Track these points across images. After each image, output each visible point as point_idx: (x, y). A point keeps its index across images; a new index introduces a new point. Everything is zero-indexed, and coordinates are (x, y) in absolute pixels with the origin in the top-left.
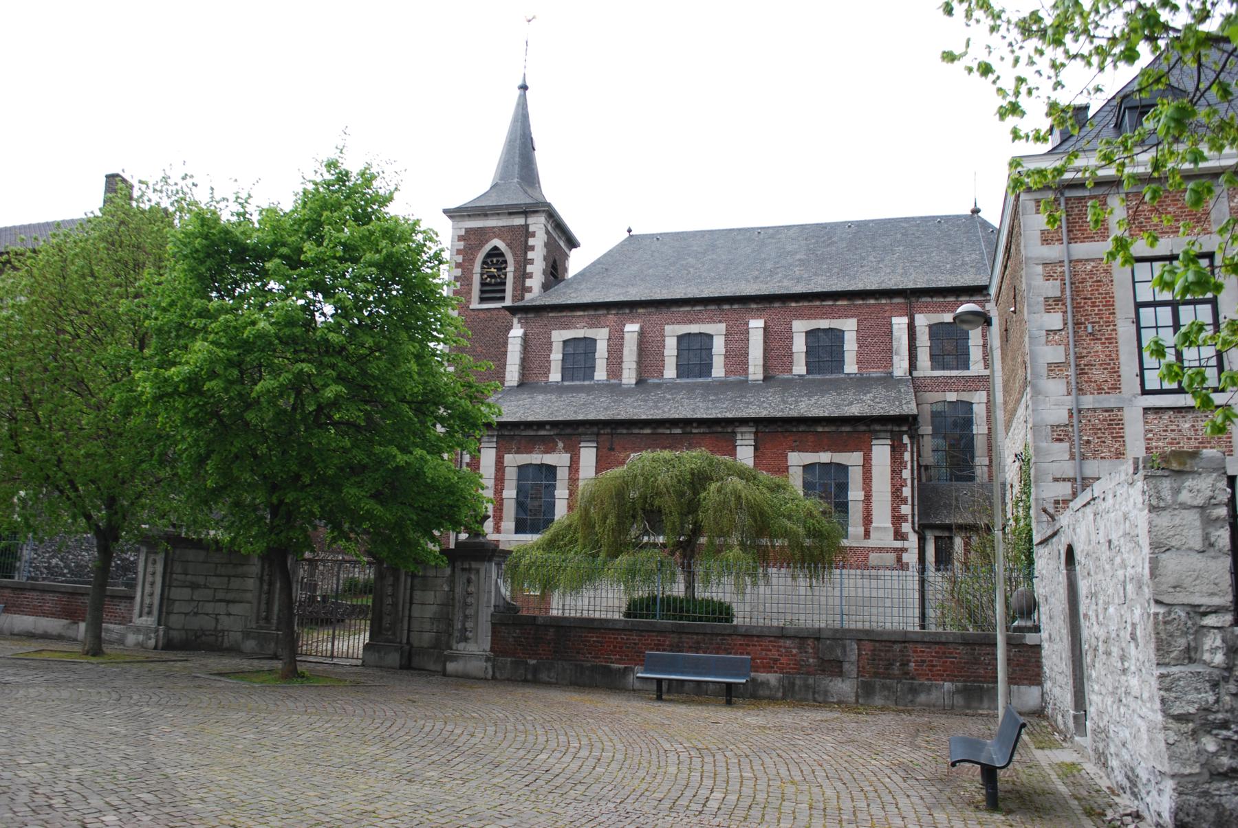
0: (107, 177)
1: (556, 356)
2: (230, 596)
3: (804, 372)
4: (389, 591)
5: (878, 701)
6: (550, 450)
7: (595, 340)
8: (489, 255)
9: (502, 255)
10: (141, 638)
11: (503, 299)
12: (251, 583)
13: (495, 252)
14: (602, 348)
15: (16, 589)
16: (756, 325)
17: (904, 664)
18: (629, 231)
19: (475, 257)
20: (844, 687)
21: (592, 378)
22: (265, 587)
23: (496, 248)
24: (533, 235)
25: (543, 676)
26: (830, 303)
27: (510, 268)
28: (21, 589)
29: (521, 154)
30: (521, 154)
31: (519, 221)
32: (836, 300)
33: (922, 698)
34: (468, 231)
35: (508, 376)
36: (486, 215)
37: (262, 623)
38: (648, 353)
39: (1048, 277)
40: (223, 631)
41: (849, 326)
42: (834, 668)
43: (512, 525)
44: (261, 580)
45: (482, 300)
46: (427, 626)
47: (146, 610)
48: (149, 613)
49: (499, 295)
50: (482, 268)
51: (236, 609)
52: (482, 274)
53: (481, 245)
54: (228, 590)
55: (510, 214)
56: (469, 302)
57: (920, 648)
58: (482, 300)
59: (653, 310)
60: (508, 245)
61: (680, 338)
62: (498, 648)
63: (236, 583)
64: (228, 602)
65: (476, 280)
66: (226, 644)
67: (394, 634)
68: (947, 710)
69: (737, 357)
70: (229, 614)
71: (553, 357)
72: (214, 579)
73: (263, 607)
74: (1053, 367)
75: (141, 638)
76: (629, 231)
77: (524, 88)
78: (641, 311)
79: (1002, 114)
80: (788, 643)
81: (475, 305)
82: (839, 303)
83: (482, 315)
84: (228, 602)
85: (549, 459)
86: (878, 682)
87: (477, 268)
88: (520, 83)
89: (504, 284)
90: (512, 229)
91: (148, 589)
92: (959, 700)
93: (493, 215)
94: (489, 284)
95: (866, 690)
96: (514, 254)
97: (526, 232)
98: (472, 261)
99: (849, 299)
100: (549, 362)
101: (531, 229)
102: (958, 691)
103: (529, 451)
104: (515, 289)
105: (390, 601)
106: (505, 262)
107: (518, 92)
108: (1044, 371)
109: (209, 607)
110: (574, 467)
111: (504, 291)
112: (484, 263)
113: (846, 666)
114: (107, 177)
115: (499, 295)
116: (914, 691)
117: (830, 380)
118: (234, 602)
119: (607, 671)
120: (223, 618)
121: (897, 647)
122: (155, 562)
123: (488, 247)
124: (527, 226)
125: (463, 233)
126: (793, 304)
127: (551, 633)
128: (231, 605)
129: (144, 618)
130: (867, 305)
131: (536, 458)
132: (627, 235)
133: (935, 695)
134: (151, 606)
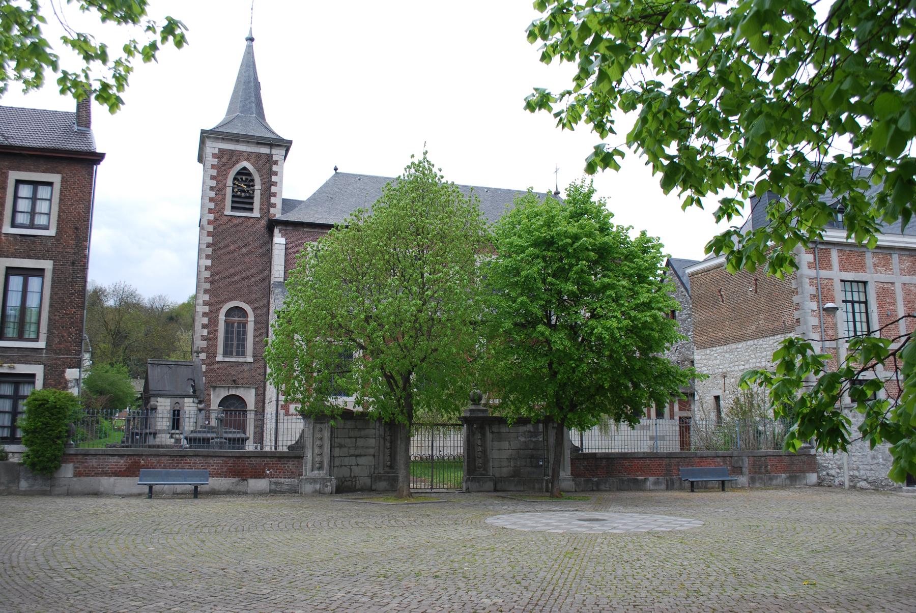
0: (290, 142)
2: (357, 452)
4: (479, 442)
5: (758, 485)
8: (238, 173)
9: (250, 174)
10: (318, 486)
11: (251, 210)
12: (372, 442)
13: (244, 172)
15: (176, 456)
17: (766, 467)
18: (336, 169)
19: (228, 173)
20: (743, 480)
22: (388, 445)
23: (245, 168)
25: (602, 487)
27: (258, 186)
28: (180, 456)
29: (248, 92)
30: (248, 92)
31: (265, 150)
33: (774, 482)
34: (221, 151)
36: (238, 141)
37: (387, 469)
39: (811, 285)
40: (355, 477)
42: (738, 470)
44: (385, 439)
45: (233, 208)
46: (505, 463)
48: (320, 468)
49: (247, 206)
51: (361, 461)
53: (233, 164)
55: (258, 143)
56: (223, 208)
57: (772, 458)
58: (233, 208)
60: (255, 168)
62: (575, 474)
63: (361, 442)
64: (356, 456)
65: (229, 191)
66: (358, 487)
67: (485, 469)
68: (783, 487)
72: (348, 440)
73: (388, 458)
74: (814, 327)
75: (318, 486)
76: (336, 169)
77: (251, 39)
79: (247, 39)
80: (719, 460)
83: (234, 221)
84: (356, 456)
86: (757, 476)
87: (230, 182)
88: (247, 35)
89: (252, 198)
90: (258, 155)
91: (317, 451)
92: (788, 482)
93: (243, 142)
94: (238, 197)
95: (752, 480)
96: (261, 176)
98: (225, 176)
101: (275, 158)
102: (788, 478)
104: (262, 203)
105: (480, 449)
106: (253, 180)
107: (245, 43)
108: (811, 329)
109: (347, 461)
111: (252, 204)
112: (235, 179)
113: (744, 469)
114: (290, 142)
115: (247, 206)
116: (771, 479)
118: (360, 456)
119: (636, 481)
120: (355, 468)
121: (763, 459)
122: (321, 430)
123: (238, 167)
124: (271, 155)
125: (216, 151)
127: (604, 462)
133: (779, 480)
134: (321, 463)
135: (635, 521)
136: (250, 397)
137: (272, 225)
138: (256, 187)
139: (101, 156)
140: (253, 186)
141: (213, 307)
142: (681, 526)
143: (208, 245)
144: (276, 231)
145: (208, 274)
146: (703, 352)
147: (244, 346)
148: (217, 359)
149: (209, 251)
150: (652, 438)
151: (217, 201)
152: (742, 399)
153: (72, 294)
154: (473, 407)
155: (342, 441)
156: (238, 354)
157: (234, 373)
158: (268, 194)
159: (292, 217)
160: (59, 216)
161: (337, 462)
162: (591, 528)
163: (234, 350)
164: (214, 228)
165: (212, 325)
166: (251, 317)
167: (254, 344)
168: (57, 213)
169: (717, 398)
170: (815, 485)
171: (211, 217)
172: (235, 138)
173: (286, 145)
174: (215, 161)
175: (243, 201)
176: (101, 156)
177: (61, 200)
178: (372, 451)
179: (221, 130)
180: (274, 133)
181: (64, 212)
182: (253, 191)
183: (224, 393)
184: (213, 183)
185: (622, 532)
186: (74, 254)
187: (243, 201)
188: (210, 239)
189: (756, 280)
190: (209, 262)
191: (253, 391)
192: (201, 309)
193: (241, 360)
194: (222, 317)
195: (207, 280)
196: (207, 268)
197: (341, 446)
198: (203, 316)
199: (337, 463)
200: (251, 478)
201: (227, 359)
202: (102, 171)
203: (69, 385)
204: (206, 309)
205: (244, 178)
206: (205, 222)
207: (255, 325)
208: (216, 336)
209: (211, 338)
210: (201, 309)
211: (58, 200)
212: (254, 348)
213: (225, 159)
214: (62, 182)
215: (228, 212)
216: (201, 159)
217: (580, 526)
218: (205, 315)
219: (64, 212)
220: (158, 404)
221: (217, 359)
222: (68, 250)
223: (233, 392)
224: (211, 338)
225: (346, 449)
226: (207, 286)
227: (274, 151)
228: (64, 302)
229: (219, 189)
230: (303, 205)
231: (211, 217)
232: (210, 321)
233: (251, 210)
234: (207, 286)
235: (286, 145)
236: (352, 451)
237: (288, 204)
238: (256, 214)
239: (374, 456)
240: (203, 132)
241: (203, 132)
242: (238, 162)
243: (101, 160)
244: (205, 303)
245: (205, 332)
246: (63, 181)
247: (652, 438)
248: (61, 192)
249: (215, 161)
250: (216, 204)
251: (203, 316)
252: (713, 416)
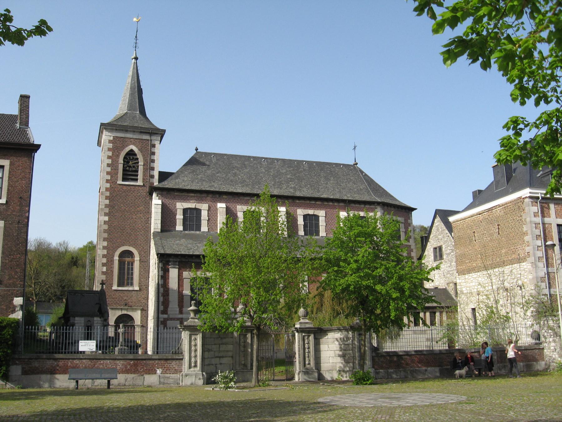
0: (164, 131)
1: (180, 217)
3: (303, 234)
7: (201, 210)
9: (135, 155)
11: (137, 180)
13: (131, 153)
15: (93, 359)
16: (221, 206)
18: (197, 149)
21: (200, 230)
23: (132, 150)
26: (314, 202)
31: (147, 137)
32: (317, 201)
38: (167, 216)
41: (321, 213)
45: (124, 179)
47: (193, 365)
50: (124, 161)
52: (124, 165)
53: (124, 147)
54: (219, 351)
55: (141, 132)
56: (117, 180)
59: (231, 197)
63: (223, 348)
64: (220, 357)
65: (121, 167)
69: (212, 220)
70: (221, 364)
71: (178, 217)
76: (197, 149)
77: (136, 58)
78: (224, 197)
81: (120, 182)
82: (317, 203)
83: (125, 188)
84: (220, 357)
87: (121, 161)
89: (137, 171)
93: (131, 131)
94: (129, 171)
96: (143, 156)
98: (118, 156)
99: (322, 202)
100: (175, 219)
104: (144, 175)
106: (137, 159)
111: (137, 175)
114: (164, 131)
117: (190, 235)
118: (223, 357)
123: (127, 149)
125: (112, 138)
126: (297, 201)
128: (221, 359)
129: (192, 369)
130: (329, 205)
132: (195, 151)
134: (196, 362)
135: (420, 398)
136: (137, 316)
137: (153, 189)
138: (139, 164)
139: (38, 147)
140: (138, 163)
141: (110, 250)
142: (452, 400)
143: (106, 206)
144: (154, 195)
145: (106, 227)
146: (462, 277)
147: (132, 279)
148: (113, 288)
149: (107, 210)
150: (428, 340)
151: (113, 174)
152: (356, 320)
153: (18, 244)
155: (209, 347)
156: (128, 285)
157: (125, 298)
158: (149, 168)
159: (168, 184)
160: (8, 190)
161: (207, 362)
162: (391, 403)
163: (126, 282)
164: (110, 194)
165: (109, 264)
166: (137, 258)
167: (140, 277)
168: (7, 187)
169: (474, 310)
171: (108, 185)
172: (125, 129)
173: (161, 133)
174: (111, 146)
175: (130, 173)
176: (38, 147)
177: (9, 178)
178: (230, 354)
179: (115, 123)
180: (153, 125)
181: (12, 186)
182: (138, 167)
183: (119, 313)
184: (110, 161)
185: (412, 405)
186: (19, 216)
187: (130, 173)
188: (107, 202)
189: (498, 225)
190: (106, 218)
191: (139, 312)
192: (100, 252)
193: (131, 288)
194: (116, 258)
195: (105, 231)
196: (105, 222)
197: (209, 350)
198: (103, 257)
199: (206, 363)
200: (146, 374)
201: (120, 288)
202: (38, 156)
203: (16, 309)
204: (105, 252)
205: (131, 158)
206: (103, 190)
207: (140, 263)
208: (112, 272)
209: (109, 273)
210: (100, 252)
211: (7, 179)
212: (140, 280)
213: (117, 145)
214: (10, 165)
215: (120, 182)
216: (99, 144)
217: (384, 402)
218: (104, 256)
219: (12, 186)
220: (76, 322)
221: (113, 288)
222: (14, 213)
223: (124, 312)
224: (109, 273)
225: (212, 353)
227: (153, 138)
228: (12, 250)
229: (113, 165)
230: (173, 176)
231: (108, 185)
232: (108, 261)
233: (137, 180)
234: (106, 235)
235: (161, 133)
237: (164, 176)
238: (140, 183)
239: (232, 357)
240: (102, 125)
241: (102, 125)
242: (127, 146)
243: (38, 149)
244: (104, 248)
246: (11, 164)
247: (428, 340)
248: (10, 172)
249: (111, 146)
250: (112, 177)
251: (103, 257)
252: (472, 323)
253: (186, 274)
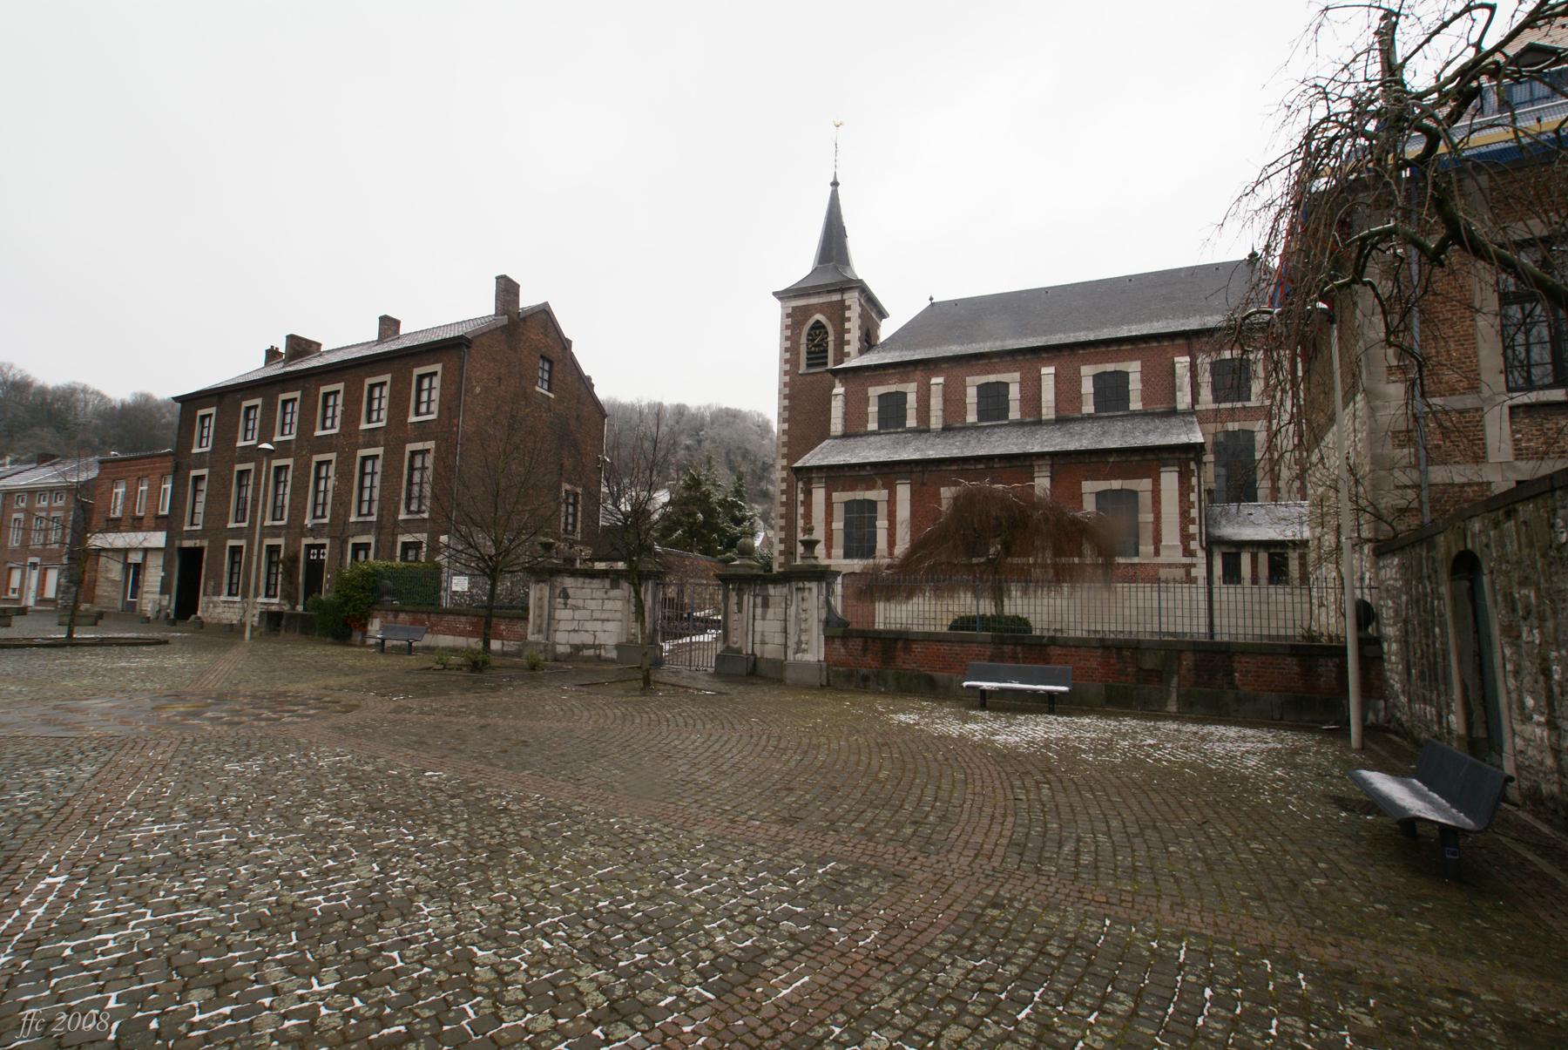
1: (873, 409)
2: (605, 616)
6: (870, 487)
8: (813, 328)
13: (818, 326)
14: (912, 399)
23: (818, 322)
24: (849, 308)
27: (831, 338)
31: (836, 297)
35: (833, 428)
43: (841, 552)
61: (980, 388)
65: (803, 349)
77: (835, 184)
83: (809, 379)
85: (870, 495)
87: (804, 340)
96: (834, 325)
97: (842, 307)
103: (852, 489)
107: (830, 189)
110: (892, 502)
123: (811, 322)
124: (843, 301)
131: (860, 495)
154: (266, 600)
170: (915, 641)
178: (619, 615)
226: (785, 450)
236: (596, 615)
238: (205, 543)
245: (784, 498)
253: (836, 496)
